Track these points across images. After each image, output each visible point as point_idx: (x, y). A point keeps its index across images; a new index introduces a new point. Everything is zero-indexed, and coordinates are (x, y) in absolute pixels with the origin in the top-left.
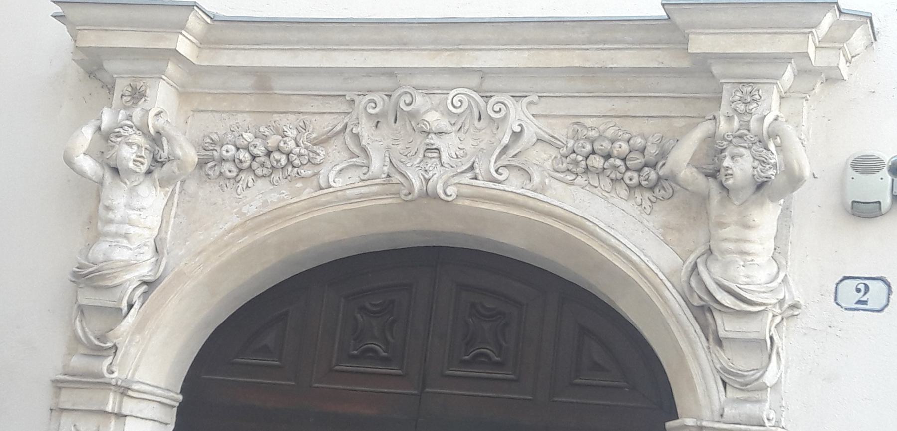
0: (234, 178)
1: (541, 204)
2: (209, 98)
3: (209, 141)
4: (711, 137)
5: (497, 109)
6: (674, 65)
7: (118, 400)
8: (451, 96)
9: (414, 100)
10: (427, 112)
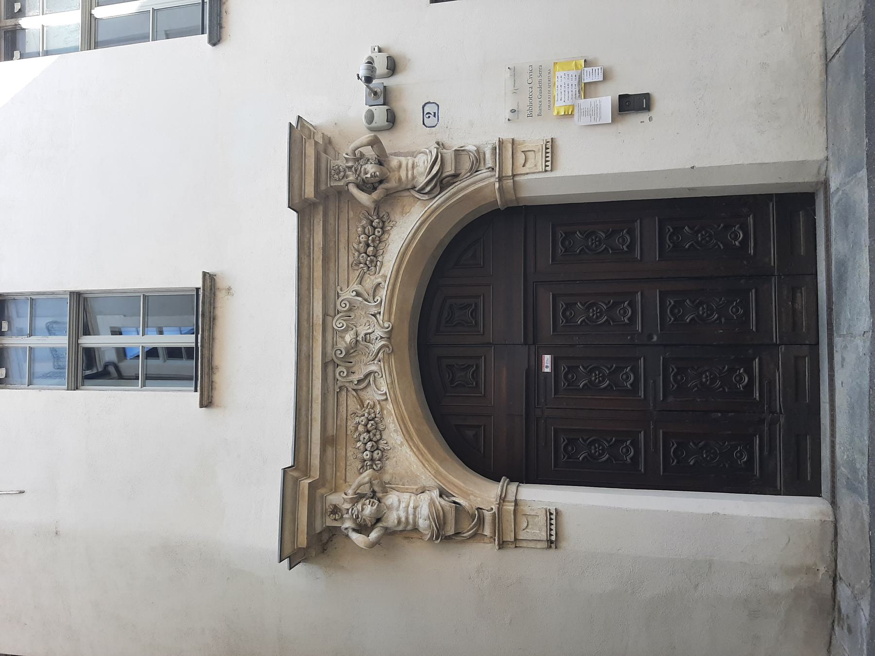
0: (382, 452)
1: (393, 276)
2: (338, 474)
4: (358, 187)
5: (344, 305)
6: (321, 213)
7: (507, 503)
9: (339, 348)
10: (346, 342)
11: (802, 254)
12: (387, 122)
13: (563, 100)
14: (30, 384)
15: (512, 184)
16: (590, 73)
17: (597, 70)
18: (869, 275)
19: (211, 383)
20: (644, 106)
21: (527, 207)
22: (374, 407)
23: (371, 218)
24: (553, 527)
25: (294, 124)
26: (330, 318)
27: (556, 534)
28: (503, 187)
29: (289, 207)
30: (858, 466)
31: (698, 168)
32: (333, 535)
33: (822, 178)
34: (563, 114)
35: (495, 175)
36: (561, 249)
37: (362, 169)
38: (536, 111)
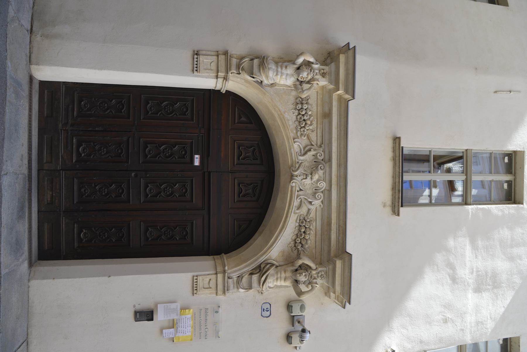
0: (296, 108)
3: (308, 98)
4: (310, 268)
5: (319, 196)
6: (332, 251)
7: (223, 76)
8: (323, 182)
9: (325, 169)
11: (46, 224)
12: (292, 306)
13: (187, 319)
14: (491, 153)
15: (217, 269)
16: (171, 334)
17: (166, 335)
18: (2, 209)
19: (394, 151)
20: (138, 314)
21: (208, 254)
22: (302, 135)
23: (302, 249)
24: (195, 66)
25: (347, 304)
26: (327, 188)
27: (194, 59)
28: (223, 267)
29: (351, 255)
30: (13, 95)
31: (106, 276)
32: (324, 61)
33: (33, 269)
34: (187, 310)
35: (228, 274)
36: (188, 229)
37: (308, 278)
38: (203, 312)
